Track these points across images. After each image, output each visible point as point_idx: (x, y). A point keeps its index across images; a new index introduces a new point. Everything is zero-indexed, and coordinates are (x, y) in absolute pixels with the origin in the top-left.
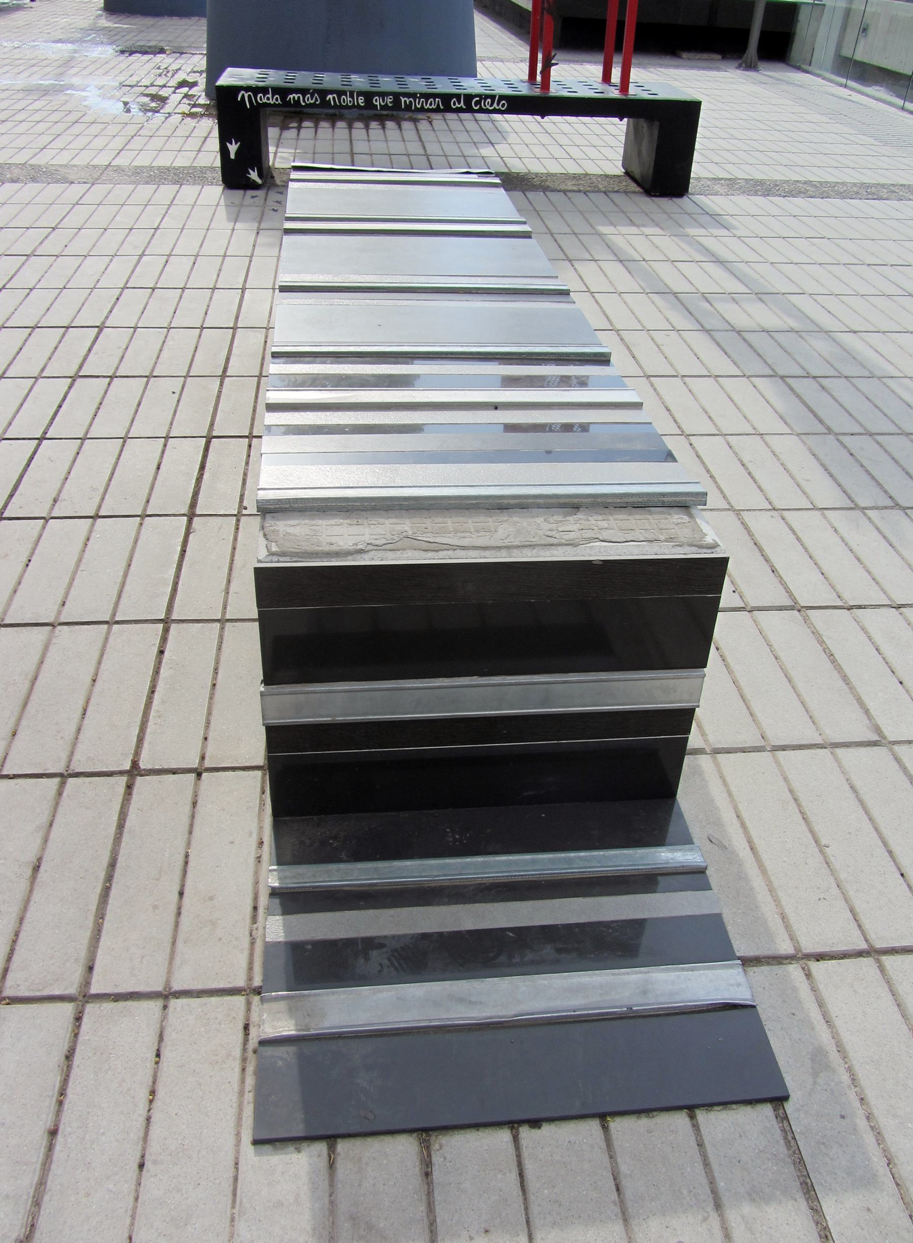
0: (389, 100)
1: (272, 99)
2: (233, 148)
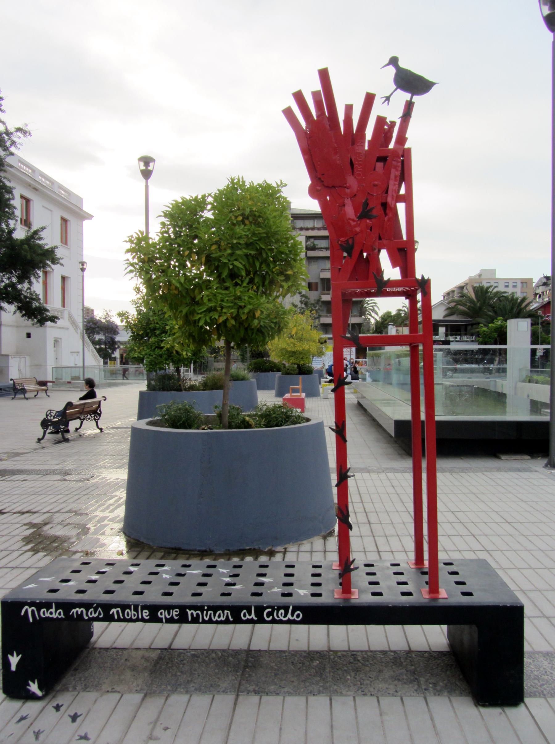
0: (175, 613)
1: (55, 614)
2: (14, 660)
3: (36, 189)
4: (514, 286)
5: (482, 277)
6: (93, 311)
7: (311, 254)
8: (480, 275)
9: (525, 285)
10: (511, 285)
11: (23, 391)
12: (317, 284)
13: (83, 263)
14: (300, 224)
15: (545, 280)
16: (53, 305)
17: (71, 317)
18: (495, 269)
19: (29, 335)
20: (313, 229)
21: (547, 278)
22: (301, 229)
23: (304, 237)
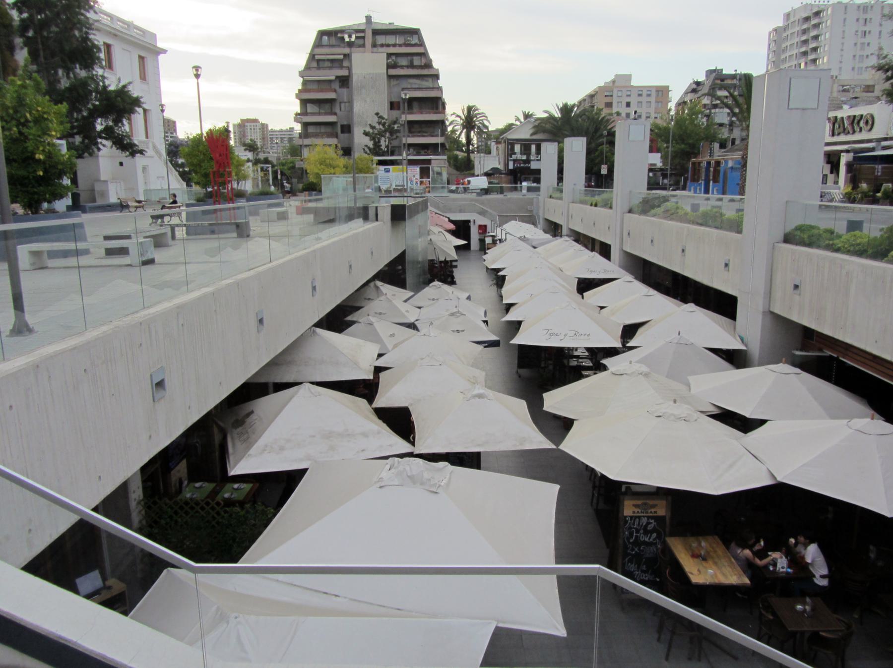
3: (116, 35)
4: (649, 95)
5: (617, 84)
6: (174, 122)
7: (393, 72)
8: (614, 82)
9: (660, 93)
10: (645, 93)
11: (127, 207)
12: (399, 103)
13: (162, 106)
14: (381, 39)
15: (694, 86)
16: (138, 138)
17: (154, 147)
18: (630, 76)
19: (121, 164)
20: (394, 45)
21: (698, 84)
22: (382, 45)
23: (385, 55)
